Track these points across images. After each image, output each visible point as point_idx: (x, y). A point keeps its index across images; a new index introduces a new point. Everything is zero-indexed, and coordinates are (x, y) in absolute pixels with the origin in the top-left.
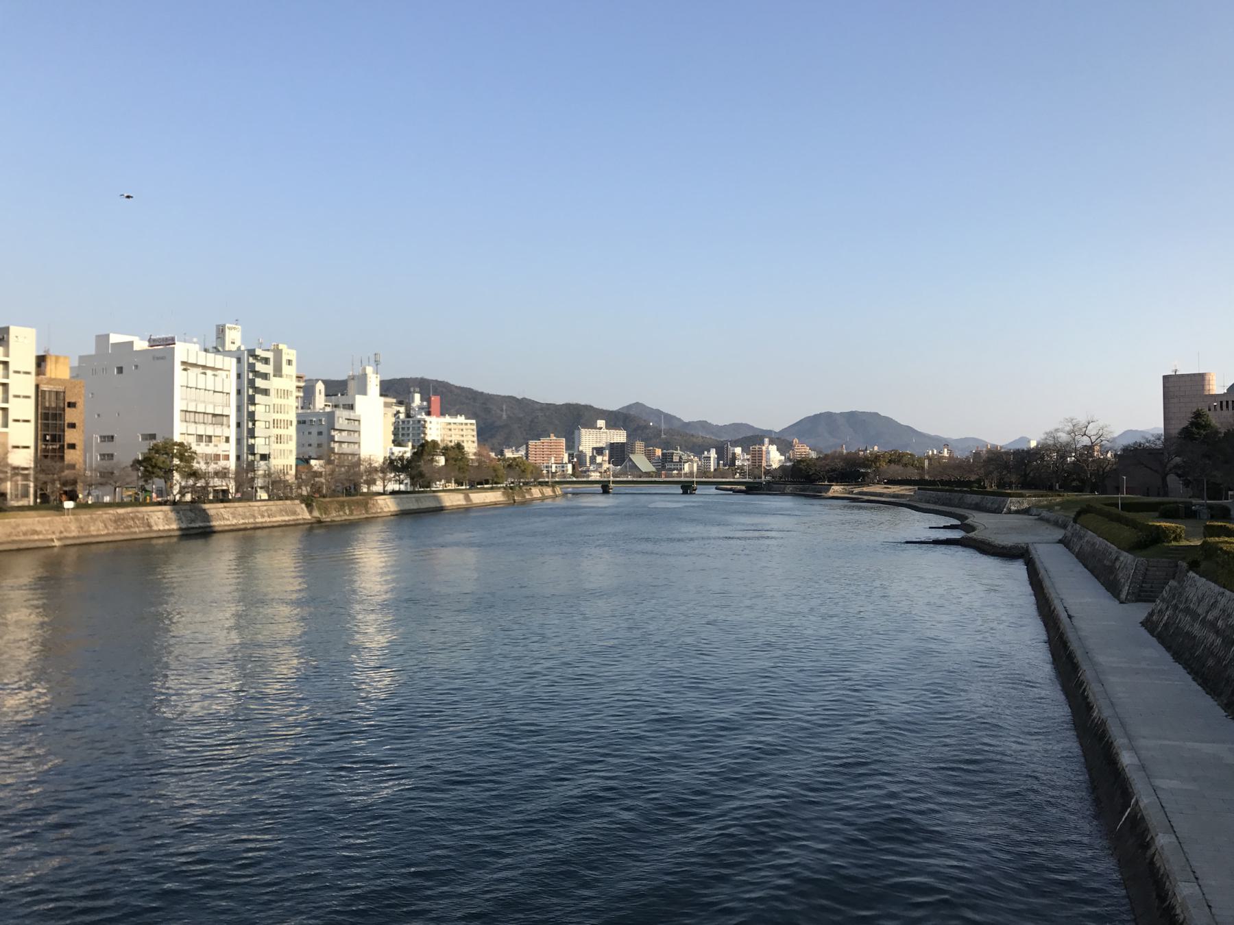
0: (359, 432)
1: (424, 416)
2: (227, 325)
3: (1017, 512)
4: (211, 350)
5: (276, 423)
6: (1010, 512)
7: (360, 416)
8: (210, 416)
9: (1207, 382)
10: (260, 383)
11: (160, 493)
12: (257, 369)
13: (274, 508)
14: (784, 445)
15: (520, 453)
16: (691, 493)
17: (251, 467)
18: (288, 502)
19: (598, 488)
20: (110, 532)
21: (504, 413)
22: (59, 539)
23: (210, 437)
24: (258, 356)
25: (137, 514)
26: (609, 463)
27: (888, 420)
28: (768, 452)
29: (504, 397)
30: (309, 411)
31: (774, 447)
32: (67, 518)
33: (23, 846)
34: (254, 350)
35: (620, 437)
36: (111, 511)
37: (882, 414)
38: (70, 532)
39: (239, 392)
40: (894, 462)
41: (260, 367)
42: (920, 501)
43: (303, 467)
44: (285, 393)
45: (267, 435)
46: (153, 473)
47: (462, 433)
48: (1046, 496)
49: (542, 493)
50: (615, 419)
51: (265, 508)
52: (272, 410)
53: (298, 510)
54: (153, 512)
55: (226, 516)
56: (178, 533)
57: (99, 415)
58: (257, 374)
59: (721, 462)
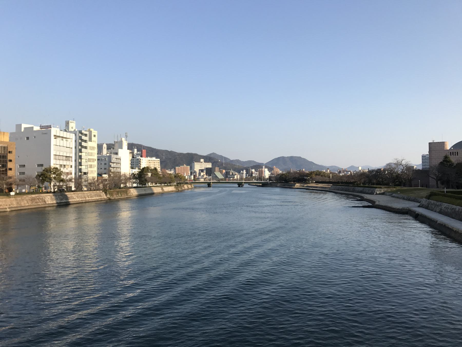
0: (120, 163)
1: (140, 157)
2: (70, 121)
3: (379, 194)
4: (63, 130)
5: (90, 160)
6: (377, 194)
7: (120, 157)
8: (65, 157)
9: (445, 145)
10: (83, 144)
11: (46, 188)
12: (82, 138)
13: (92, 194)
14: (270, 169)
15: (171, 171)
16: (241, 187)
17: (80, 177)
18: (98, 191)
19: (206, 185)
20: (29, 204)
21: (164, 157)
22: (9, 208)
23: (65, 165)
24: (83, 133)
25: (40, 197)
26: (207, 175)
27: (304, 160)
28: (265, 171)
29: (164, 150)
30: (101, 155)
31: (267, 169)
32: (12, 199)
34: (81, 131)
35: (209, 165)
36: (30, 196)
37: (302, 157)
38: (13, 205)
39: (75, 148)
40: (318, 175)
41: (84, 138)
42: (335, 190)
43: (100, 177)
44: (93, 148)
45: (87, 165)
46: (45, 180)
47: (154, 164)
48: (390, 188)
49: (188, 187)
50: (208, 159)
51: (89, 194)
52: (88, 155)
53: (102, 195)
54: (46, 196)
55: (75, 198)
56: (56, 205)
57: (18, 157)
58: (82, 140)
59: (247, 175)
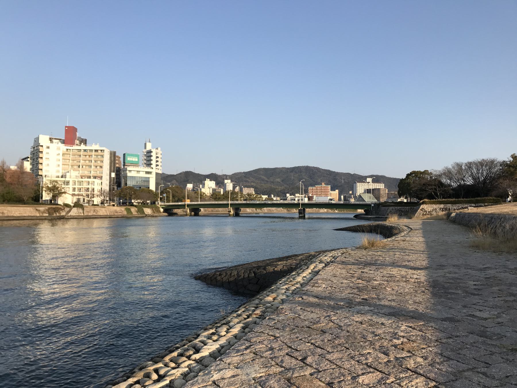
21: (343, 180)
33: (476, 205)
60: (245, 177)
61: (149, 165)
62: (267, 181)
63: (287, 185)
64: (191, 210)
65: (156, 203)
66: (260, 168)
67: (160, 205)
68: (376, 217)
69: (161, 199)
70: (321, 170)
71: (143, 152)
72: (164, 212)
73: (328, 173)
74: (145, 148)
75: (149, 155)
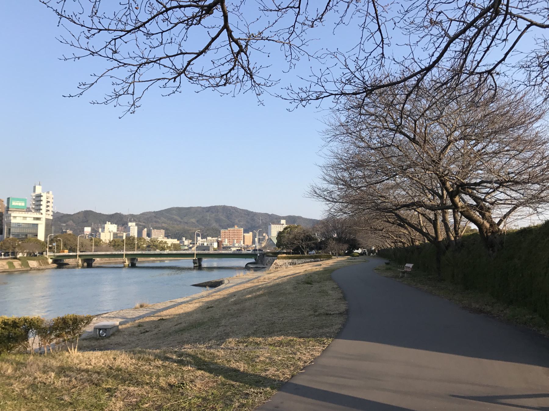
21: (261, 221)
60: (155, 217)
61: (38, 210)
62: (180, 222)
63: (203, 225)
64: (84, 261)
65: (45, 253)
66: (172, 207)
67: (49, 256)
68: (256, 267)
69: (50, 248)
70: (239, 210)
71: (32, 196)
72: (52, 263)
73: (246, 213)
74: (34, 191)
75: (38, 199)
